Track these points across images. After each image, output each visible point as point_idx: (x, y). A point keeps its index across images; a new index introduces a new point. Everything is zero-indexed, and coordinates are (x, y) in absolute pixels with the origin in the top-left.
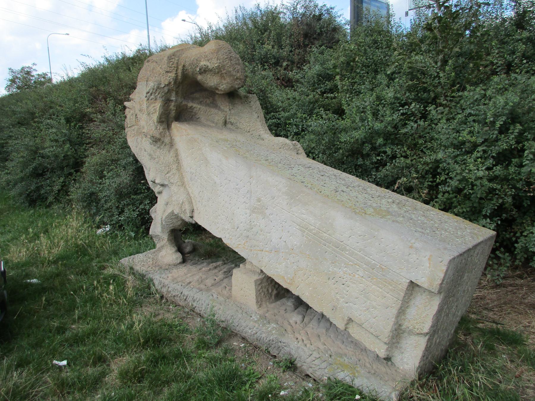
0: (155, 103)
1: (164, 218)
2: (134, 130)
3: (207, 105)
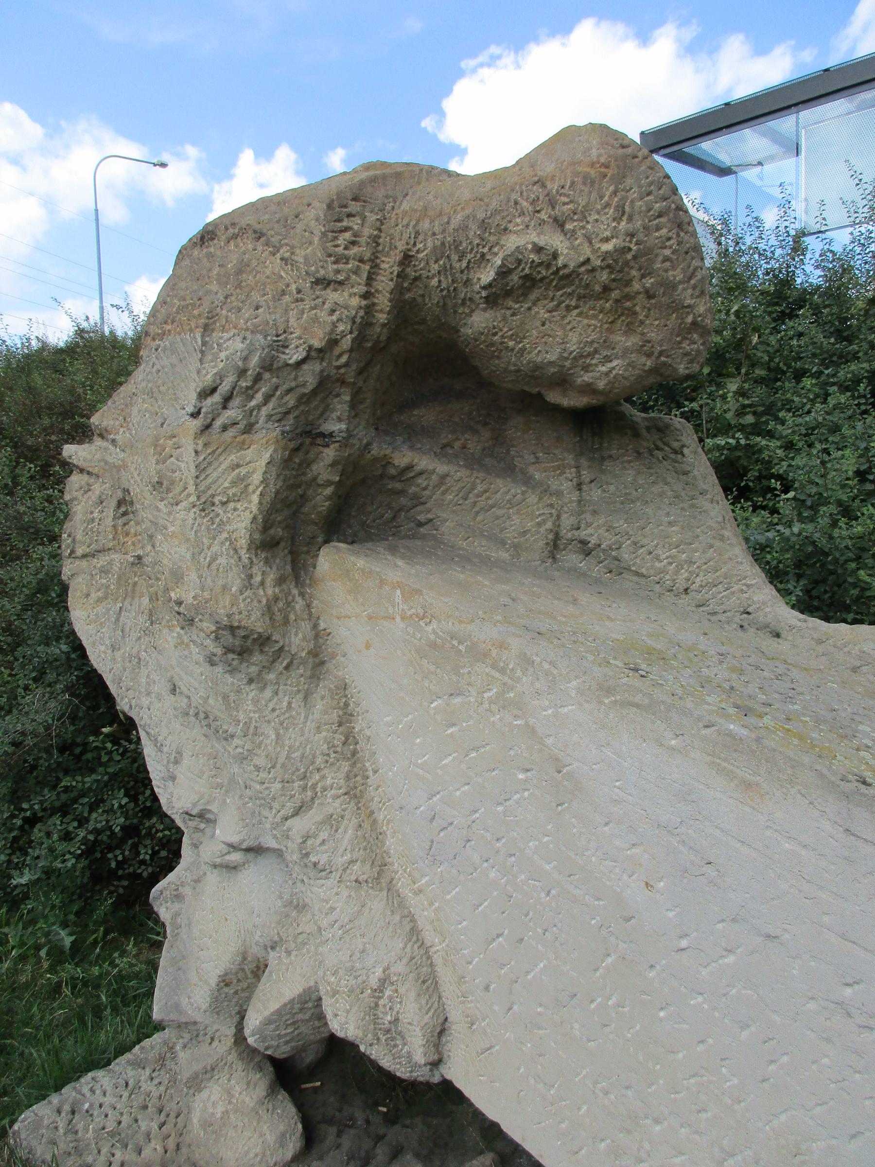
0: (242, 446)
2: (104, 571)
3: (474, 462)
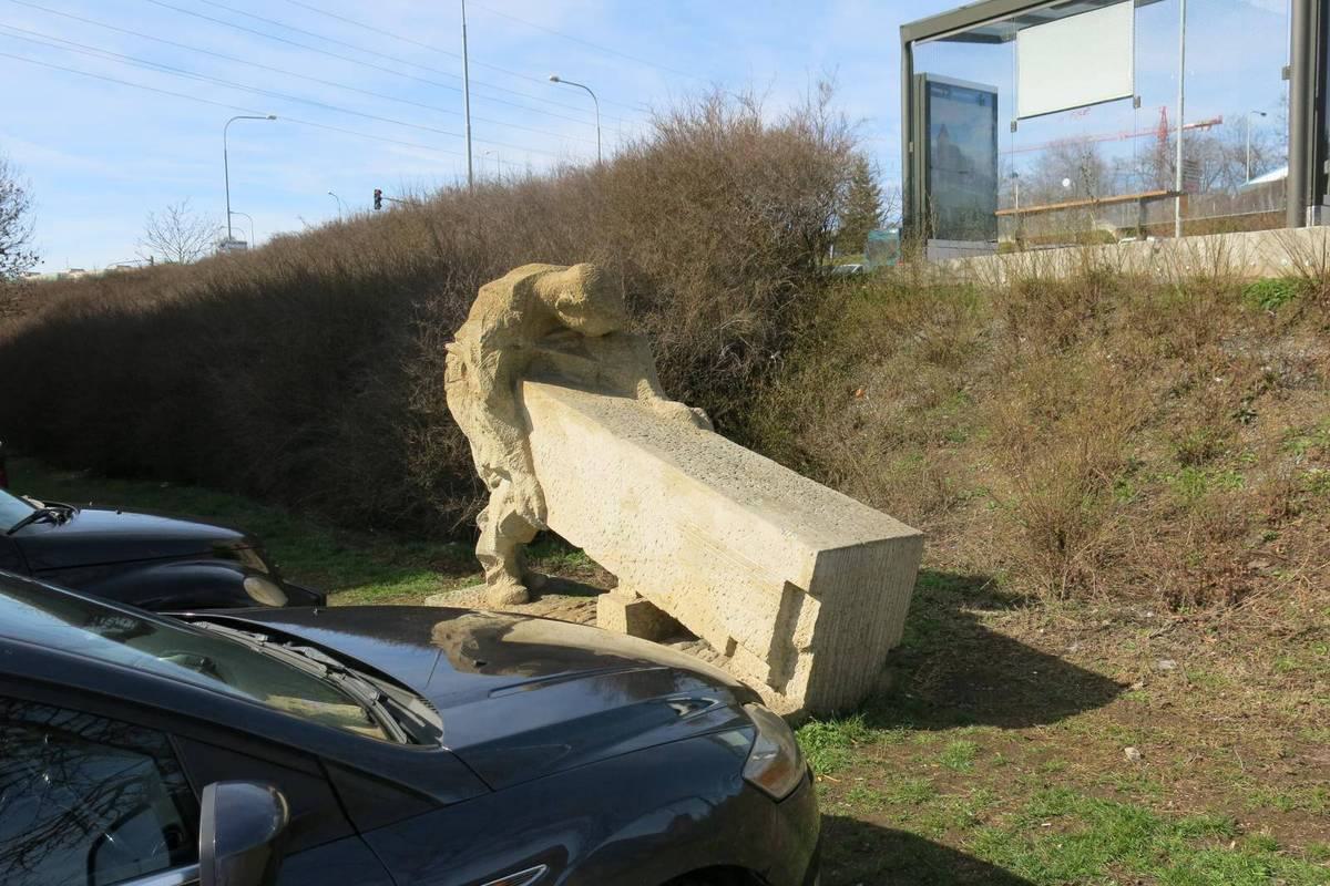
1: (501, 521)
